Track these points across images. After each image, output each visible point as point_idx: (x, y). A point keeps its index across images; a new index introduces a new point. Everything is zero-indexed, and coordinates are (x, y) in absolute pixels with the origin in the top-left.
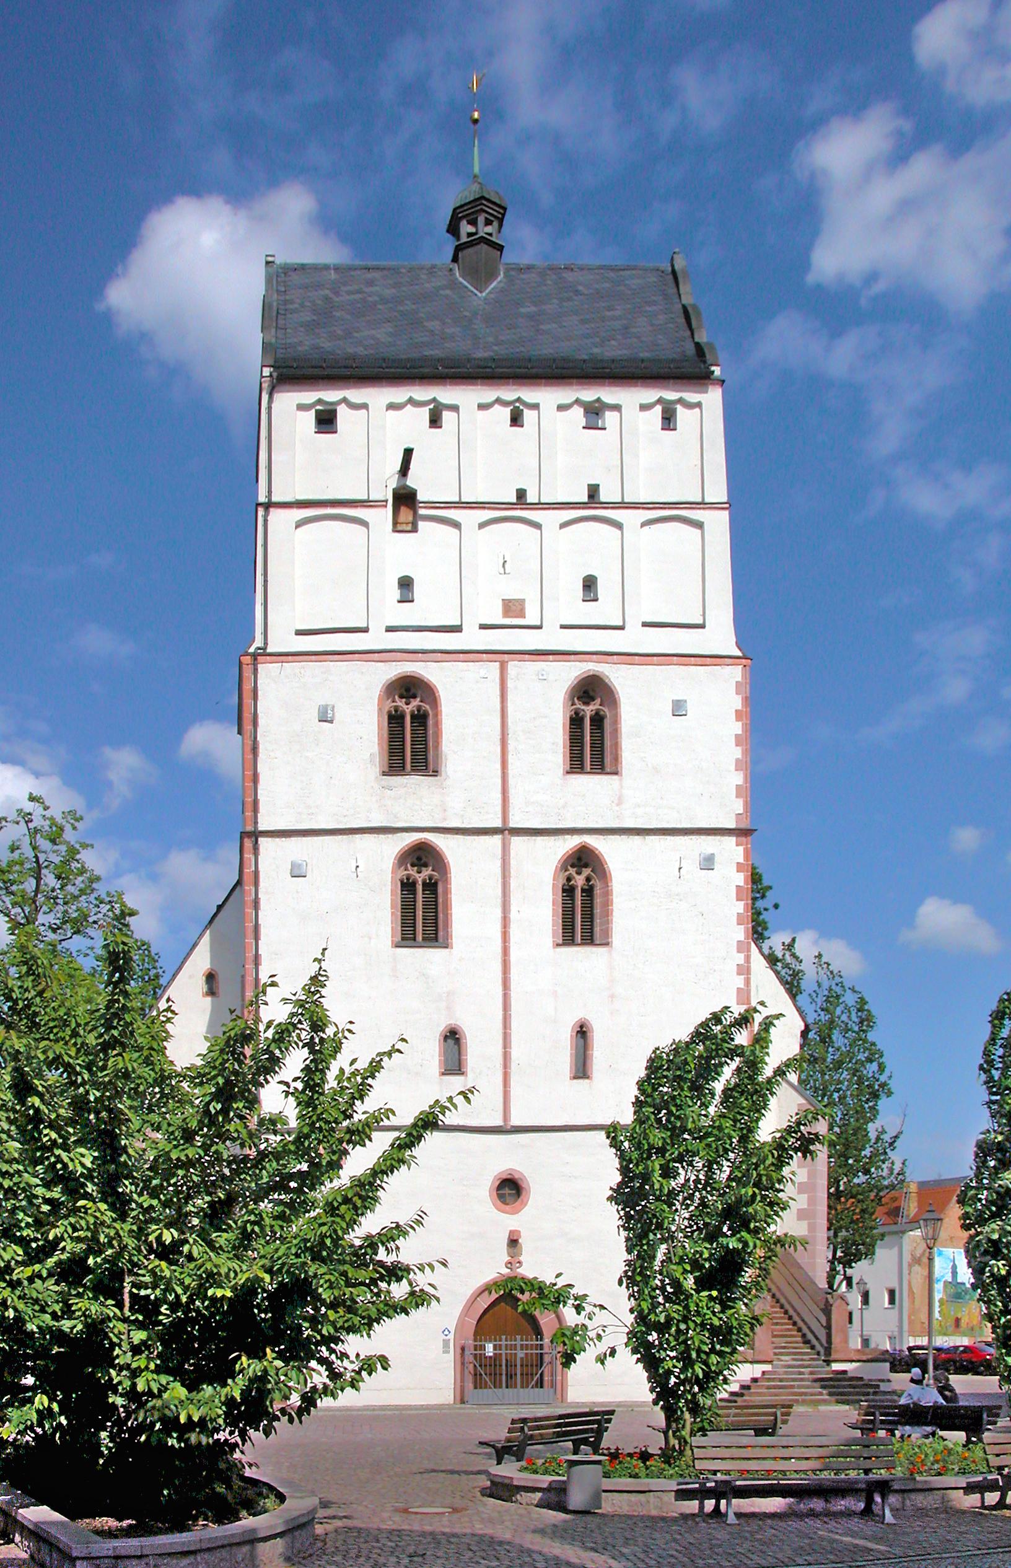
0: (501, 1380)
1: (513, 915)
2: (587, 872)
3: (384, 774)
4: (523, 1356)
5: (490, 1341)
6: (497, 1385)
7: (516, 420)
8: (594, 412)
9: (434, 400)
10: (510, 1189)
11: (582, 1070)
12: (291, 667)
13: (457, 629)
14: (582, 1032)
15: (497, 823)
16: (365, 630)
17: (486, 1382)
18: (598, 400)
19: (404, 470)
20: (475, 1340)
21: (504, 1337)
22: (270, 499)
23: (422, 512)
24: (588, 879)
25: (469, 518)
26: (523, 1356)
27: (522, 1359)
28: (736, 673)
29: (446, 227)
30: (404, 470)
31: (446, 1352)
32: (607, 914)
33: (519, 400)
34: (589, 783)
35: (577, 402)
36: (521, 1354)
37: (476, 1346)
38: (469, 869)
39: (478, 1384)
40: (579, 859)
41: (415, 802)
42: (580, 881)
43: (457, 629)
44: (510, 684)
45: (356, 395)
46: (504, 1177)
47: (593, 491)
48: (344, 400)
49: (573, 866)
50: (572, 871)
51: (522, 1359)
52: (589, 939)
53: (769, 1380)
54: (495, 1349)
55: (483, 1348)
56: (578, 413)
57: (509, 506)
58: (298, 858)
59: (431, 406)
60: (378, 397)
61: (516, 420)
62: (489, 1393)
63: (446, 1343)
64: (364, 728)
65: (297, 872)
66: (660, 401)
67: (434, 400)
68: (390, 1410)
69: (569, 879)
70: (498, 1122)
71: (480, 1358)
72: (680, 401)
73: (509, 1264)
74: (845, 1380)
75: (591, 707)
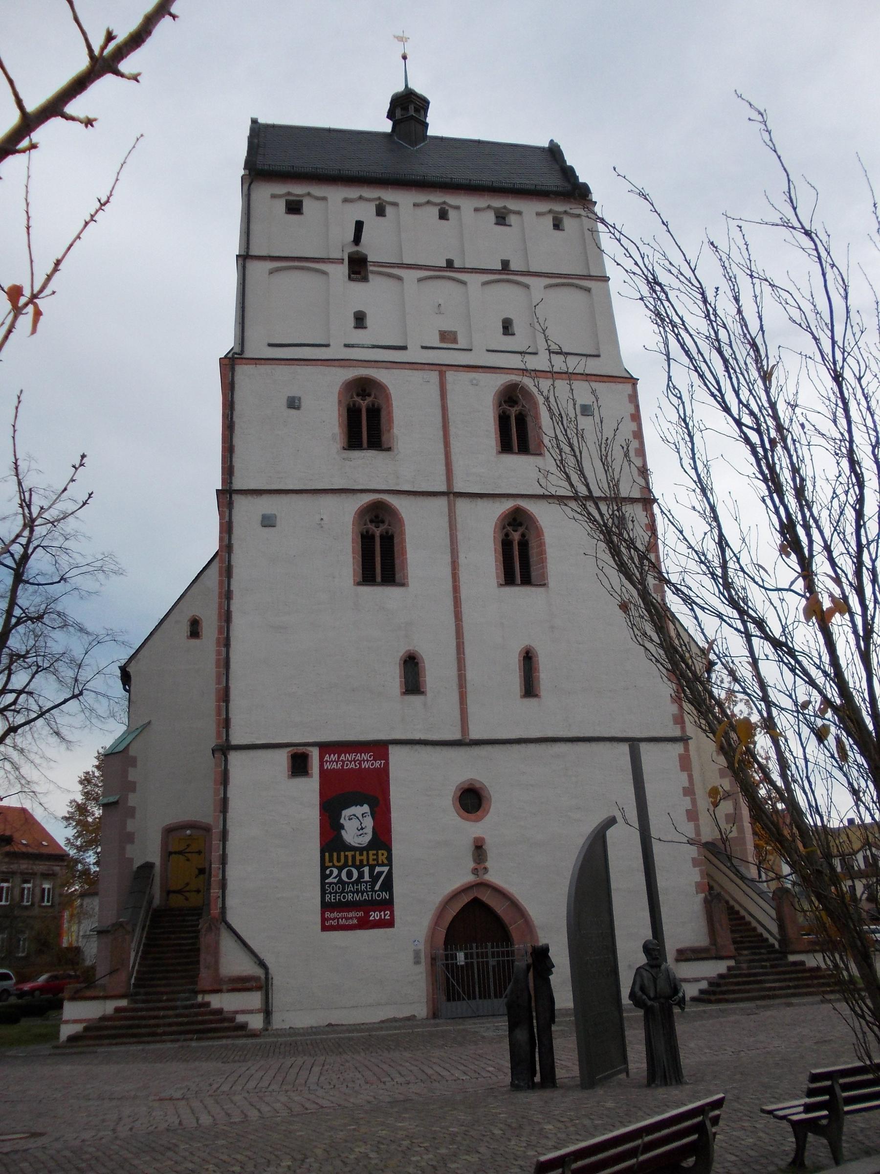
0: (474, 992)
1: (462, 560)
2: (521, 530)
3: (344, 449)
4: (495, 963)
5: (461, 950)
6: (471, 996)
7: (443, 215)
8: (501, 218)
9: (379, 198)
10: (472, 800)
11: (530, 689)
12: (263, 368)
13: (404, 348)
14: (528, 659)
15: (444, 488)
16: (327, 346)
17: (459, 993)
18: (505, 208)
19: (357, 240)
20: (446, 949)
21: (474, 945)
22: (247, 253)
23: (371, 268)
24: (523, 535)
25: (410, 276)
26: (495, 963)
27: (494, 967)
28: (506, 1018)
29: (386, 114)
30: (357, 240)
31: (417, 962)
32: (543, 561)
33: (444, 203)
34: (516, 462)
35: (489, 207)
36: (492, 962)
37: (447, 956)
38: (421, 532)
39: (452, 996)
40: (514, 519)
41: (369, 470)
42: (516, 536)
43: (404, 348)
44: (449, 387)
45: (318, 190)
46: (466, 786)
47: (505, 264)
48: (309, 194)
49: (509, 525)
50: (509, 528)
51: (494, 967)
52: (527, 581)
53: (736, 976)
54: (466, 958)
55: (454, 957)
56: (491, 217)
57: (440, 269)
58: (268, 511)
59: (377, 203)
60: (336, 194)
61: (443, 215)
62: (461, 1007)
63: (417, 954)
64: (326, 414)
65: (268, 522)
66: (550, 211)
67: (379, 198)
68: (358, 1031)
69: (507, 535)
70: (457, 736)
71: (451, 968)
72: (565, 212)
73: (475, 871)
74: (805, 971)
75: (515, 409)
